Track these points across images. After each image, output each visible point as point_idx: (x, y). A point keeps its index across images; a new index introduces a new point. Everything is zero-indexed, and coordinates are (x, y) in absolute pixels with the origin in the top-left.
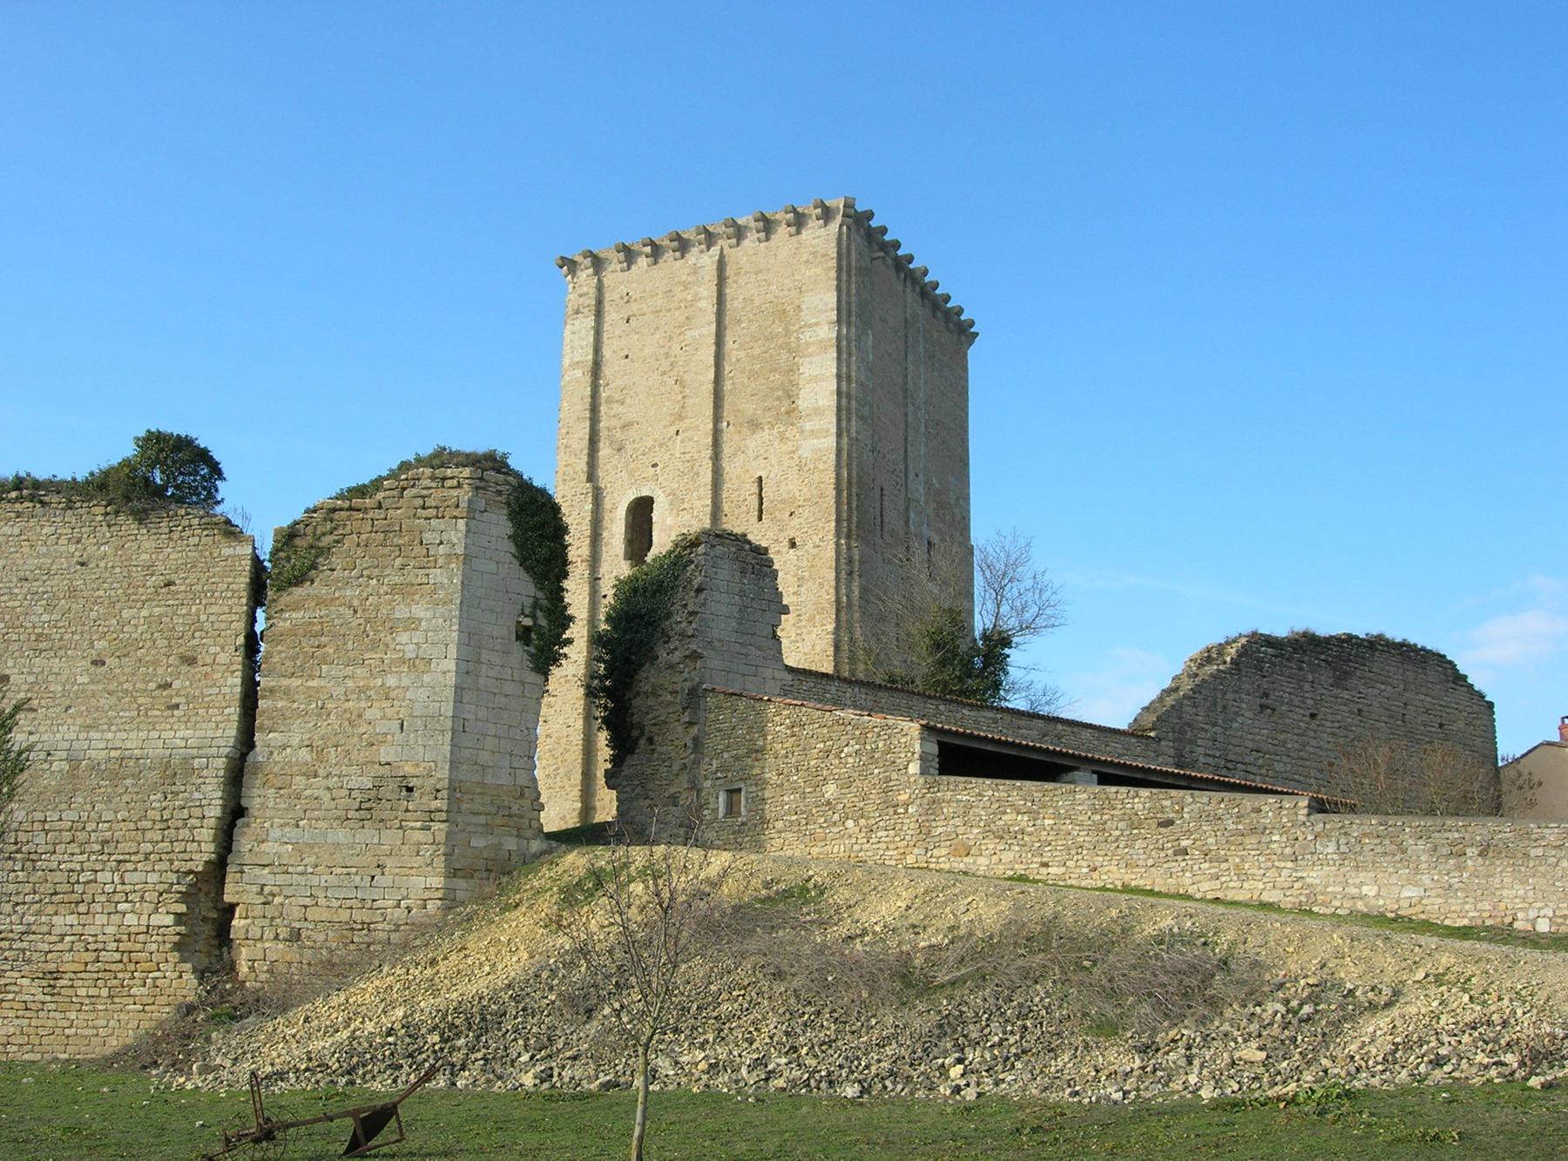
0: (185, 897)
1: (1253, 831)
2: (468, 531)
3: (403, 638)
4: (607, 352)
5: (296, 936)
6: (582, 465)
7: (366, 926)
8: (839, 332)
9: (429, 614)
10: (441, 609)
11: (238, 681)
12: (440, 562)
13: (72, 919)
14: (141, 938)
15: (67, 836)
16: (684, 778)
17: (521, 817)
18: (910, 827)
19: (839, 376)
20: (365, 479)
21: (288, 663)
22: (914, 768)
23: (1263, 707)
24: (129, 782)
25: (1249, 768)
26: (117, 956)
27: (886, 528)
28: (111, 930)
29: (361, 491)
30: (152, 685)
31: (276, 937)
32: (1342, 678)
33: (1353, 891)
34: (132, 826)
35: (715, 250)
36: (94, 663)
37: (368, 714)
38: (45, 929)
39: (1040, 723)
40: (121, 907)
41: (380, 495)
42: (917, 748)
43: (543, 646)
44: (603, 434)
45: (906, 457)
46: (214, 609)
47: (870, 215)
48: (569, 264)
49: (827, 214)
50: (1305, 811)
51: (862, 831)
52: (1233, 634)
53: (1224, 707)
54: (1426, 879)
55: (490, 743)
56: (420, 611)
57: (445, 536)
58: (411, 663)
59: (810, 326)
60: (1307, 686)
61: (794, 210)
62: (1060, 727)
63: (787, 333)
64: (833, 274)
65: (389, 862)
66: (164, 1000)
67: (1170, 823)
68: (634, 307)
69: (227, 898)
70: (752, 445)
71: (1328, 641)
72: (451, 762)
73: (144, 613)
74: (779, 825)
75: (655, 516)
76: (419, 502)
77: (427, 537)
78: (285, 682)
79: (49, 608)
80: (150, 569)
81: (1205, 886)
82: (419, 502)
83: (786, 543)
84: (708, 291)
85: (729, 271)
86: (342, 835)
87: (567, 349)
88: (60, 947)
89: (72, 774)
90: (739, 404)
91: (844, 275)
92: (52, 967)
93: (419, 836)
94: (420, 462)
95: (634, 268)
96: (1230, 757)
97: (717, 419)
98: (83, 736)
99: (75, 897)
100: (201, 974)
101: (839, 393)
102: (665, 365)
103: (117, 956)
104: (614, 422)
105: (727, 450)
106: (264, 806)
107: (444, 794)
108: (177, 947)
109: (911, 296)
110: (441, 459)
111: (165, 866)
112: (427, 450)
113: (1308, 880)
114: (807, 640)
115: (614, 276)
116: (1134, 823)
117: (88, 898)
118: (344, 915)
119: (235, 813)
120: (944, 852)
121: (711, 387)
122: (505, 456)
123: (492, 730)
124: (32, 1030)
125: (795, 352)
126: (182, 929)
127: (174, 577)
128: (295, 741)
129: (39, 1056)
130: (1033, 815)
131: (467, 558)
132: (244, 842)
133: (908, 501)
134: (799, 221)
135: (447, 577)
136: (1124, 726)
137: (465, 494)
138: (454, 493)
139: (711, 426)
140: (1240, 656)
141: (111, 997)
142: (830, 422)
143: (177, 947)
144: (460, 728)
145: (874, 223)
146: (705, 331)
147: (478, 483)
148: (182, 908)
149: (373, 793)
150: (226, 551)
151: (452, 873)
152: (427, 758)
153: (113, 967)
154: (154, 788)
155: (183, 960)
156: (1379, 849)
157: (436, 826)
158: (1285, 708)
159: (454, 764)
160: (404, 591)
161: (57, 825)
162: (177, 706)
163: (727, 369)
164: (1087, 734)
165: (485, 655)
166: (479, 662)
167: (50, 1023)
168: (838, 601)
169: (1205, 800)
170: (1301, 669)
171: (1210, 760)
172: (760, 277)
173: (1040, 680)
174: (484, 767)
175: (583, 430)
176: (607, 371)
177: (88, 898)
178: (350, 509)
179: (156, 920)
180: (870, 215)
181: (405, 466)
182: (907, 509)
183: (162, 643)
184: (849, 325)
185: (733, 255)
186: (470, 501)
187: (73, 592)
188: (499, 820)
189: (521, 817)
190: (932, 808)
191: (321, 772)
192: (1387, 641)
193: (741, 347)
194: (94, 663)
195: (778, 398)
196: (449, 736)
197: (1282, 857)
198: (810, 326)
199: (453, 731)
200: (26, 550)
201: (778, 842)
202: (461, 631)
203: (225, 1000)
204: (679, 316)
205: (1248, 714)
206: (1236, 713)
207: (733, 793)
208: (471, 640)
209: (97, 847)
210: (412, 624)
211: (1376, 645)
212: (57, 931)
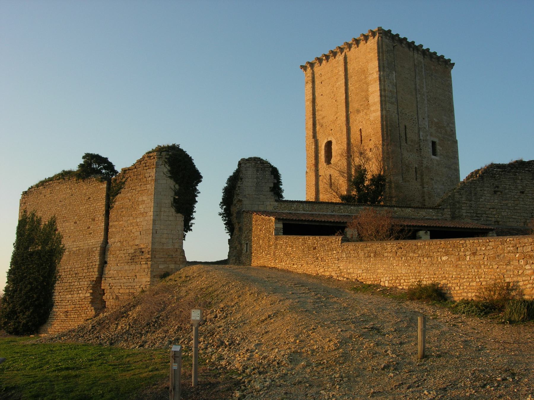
2: (156, 172)
8: (380, 75)
10: (150, 197)
11: (103, 224)
13: (70, 296)
17: (176, 258)
19: (381, 90)
25: (489, 215)
27: (408, 140)
28: (77, 298)
31: (113, 298)
34: (81, 269)
35: (343, 54)
45: (417, 113)
46: (98, 204)
49: (374, 34)
53: (476, 194)
56: (145, 198)
57: (150, 174)
60: (518, 181)
64: (377, 55)
65: (137, 274)
72: (152, 243)
73: (84, 207)
75: (333, 147)
76: (144, 165)
77: (147, 175)
78: (115, 223)
84: (342, 69)
85: (348, 60)
86: (127, 267)
90: (353, 106)
92: (66, 310)
95: (322, 65)
96: (479, 212)
102: (333, 95)
106: (110, 260)
107: (150, 253)
111: (87, 280)
115: (317, 68)
118: (128, 291)
119: (103, 263)
121: (344, 101)
123: (165, 232)
125: (368, 84)
128: (117, 241)
131: (156, 180)
133: (419, 129)
135: (151, 187)
140: (483, 173)
142: (378, 107)
144: (155, 232)
146: (342, 82)
147: (159, 156)
148: (91, 291)
151: (153, 277)
152: (145, 242)
155: (92, 306)
157: (149, 263)
158: (507, 191)
159: (153, 243)
165: (163, 209)
166: (161, 211)
170: (515, 175)
171: (469, 214)
172: (357, 60)
174: (163, 244)
176: (317, 100)
179: (86, 296)
180: (389, 31)
182: (419, 132)
184: (384, 71)
185: (348, 54)
189: (176, 258)
191: (123, 249)
195: (364, 101)
199: (152, 233)
202: (154, 203)
208: (158, 205)
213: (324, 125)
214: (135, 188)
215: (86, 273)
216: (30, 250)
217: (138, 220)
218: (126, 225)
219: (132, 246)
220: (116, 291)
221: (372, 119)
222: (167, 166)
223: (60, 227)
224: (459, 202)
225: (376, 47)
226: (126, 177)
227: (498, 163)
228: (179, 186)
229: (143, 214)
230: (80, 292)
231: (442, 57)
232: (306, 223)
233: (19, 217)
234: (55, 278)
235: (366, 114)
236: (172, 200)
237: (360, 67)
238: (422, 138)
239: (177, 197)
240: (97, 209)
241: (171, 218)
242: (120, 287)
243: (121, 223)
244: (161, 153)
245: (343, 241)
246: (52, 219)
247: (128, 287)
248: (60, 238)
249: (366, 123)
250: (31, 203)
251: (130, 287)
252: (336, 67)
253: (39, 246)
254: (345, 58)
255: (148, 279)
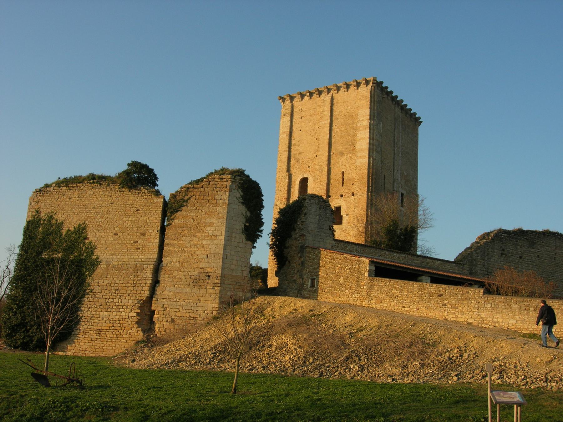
0: (140, 308)
1: (466, 299)
2: (229, 195)
3: (209, 229)
4: (294, 128)
5: (173, 321)
6: (285, 166)
7: (195, 318)
8: (370, 123)
9: (217, 222)
10: (220, 220)
11: (158, 241)
12: (221, 205)
13: (106, 313)
14: (126, 320)
15: (105, 288)
16: (298, 274)
18: (364, 293)
19: (370, 138)
20: (199, 178)
21: (173, 236)
22: (366, 274)
23: (502, 254)
24: (124, 272)
26: (119, 325)
27: (386, 189)
28: (117, 317)
29: (198, 182)
30: (132, 242)
32: (532, 244)
33: (495, 320)
34: (125, 285)
35: (330, 94)
36: (115, 234)
37: (197, 253)
38: (98, 316)
39: (421, 258)
40: (121, 310)
41: (203, 184)
42: (368, 268)
43: (252, 231)
44: (292, 156)
45: (394, 165)
46: (151, 219)
47: (382, 83)
48: (283, 99)
50: (482, 294)
51: (349, 292)
52: (492, 230)
53: (488, 254)
54: (517, 317)
55: (235, 262)
56: (214, 220)
57: (222, 197)
58: (211, 237)
59: (361, 121)
60: (519, 247)
61: (356, 81)
62: (428, 260)
63: (353, 123)
64: (369, 103)
65: (202, 299)
66: (132, 339)
67: (441, 295)
68: (303, 114)
69: (153, 308)
70: (341, 161)
71: (528, 232)
72: (222, 268)
73: (130, 219)
74: (326, 291)
76: (215, 186)
78: (172, 242)
79: (102, 217)
80: (132, 205)
81: (451, 316)
82: (215, 186)
83: (351, 194)
84: (327, 109)
85: (335, 102)
86: (188, 290)
87: (281, 128)
88: (102, 322)
89: (107, 269)
91: (372, 104)
92: (100, 328)
93: (211, 291)
94: (216, 172)
97: (329, 152)
98: (111, 257)
99: (107, 307)
100: (144, 331)
101: (370, 143)
102: (313, 133)
103: (119, 325)
104: (296, 152)
105: (332, 162)
106: (164, 280)
107: (219, 278)
108: (137, 323)
109: (397, 110)
110: (223, 171)
111: (134, 298)
112: (218, 168)
113: (482, 316)
114: (349, 230)
115: (297, 102)
116: (431, 294)
117: (111, 307)
118: (188, 315)
119: (156, 282)
120: (374, 301)
121: (327, 141)
122: (244, 171)
124: (93, 347)
125: (356, 129)
126: (139, 317)
127: (139, 208)
128: (175, 261)
129: (95, 355)
130: (401, 291)
131: (229, 204)
132: (158, 290)
134: (358, 85)
135: (222, 210)
136: (452, 259)
137: (229, 183)
138: (225, 183)
139: (327, 154)
140: (494, 237)
141: (117, 337)
142: (366, 153)
143: (137, 323)
144: (225, 257)
145: (384, 85)
146: (326, 122)
148: (139, 311)
149: (198, 277)
150: (155, 201)
151: (221, 303)
152: (215, 266)
153: (118, 328)
154: (132, 273)
155: (139, 327)
156: (503, 307)
157: (216, 288)
159: (223, 269)
160: (210, 214)
161: (102, 284)
162: (139, 248)
163: (333, 135)
164: (438, 262)
165: (234, 235)
166: (232, 237)
167: (99, 345)
168: (367, 214)
169: (452, 288)
171: (482, 272)
172: (345, 104)
173: (427, 245)
174: (232, 270)
175: (286, 155)
177: (111, 307)
178: (193, 188)
179: (131, 314)
180: (382, 83)
181: (211, 174)
182: (394, 182)
183: (135, 229)
184: (374, 121)
185: (336, 96)
186: (230, 186)
187: (109, 212)
188: (237, 287)
190: (371, 287)
191: (182, 270)
192: (550, 232)
193: (338, 128)
194: (115, 234)
195: (350, 145)
196: (221, 260)
197: (474, 308)
198: (361, 121)
199: (223, 258)
200: (95, 199)
201: (325, 296)
202: (226, 227)
203: (150, 340)
204: (318, 117)
205: (496, 256)
206: (492, 256)
207: (313, 280)
209: (114, 291)
210: (211, 224)
211: (547, 234)
212: (101, 317)
213: (300, 160)
214: (201, 208)
215: (131, 291)
216: (45, 255)
217: (204, 242)
218: (188, 245)
219: (195, 269)
220: (172, 314)
221: (358, 164)
222: (240, 191)
223: (92, 236)
224: (475, 260)
225: (368, 95)
226: (190, 195)
227: (504, 229)
228: (251, 213)
229: (213, 237)
230: (121, 310)
231: (415, 114)
232: (401, 270)
233: (28, 216)
234: (85, 291)
235: (351, 158)
236: (243, 227)
237: (348, 111)
238: (395, 189)
239: (247, 224)
240: (149, 224)
241: (241, 245)
242: (177, 310)
243: (181, 242)
244: (235, 177)
245: (484, 293)
246: (80, 225)
247: (189, 311)
248: (91, 249)
249: (350, 167)
250: (46, 204)
251: (191, 311)
252: (320, 106)
253: (59, 253)
254: (332, 99)
255: (216, 305)
